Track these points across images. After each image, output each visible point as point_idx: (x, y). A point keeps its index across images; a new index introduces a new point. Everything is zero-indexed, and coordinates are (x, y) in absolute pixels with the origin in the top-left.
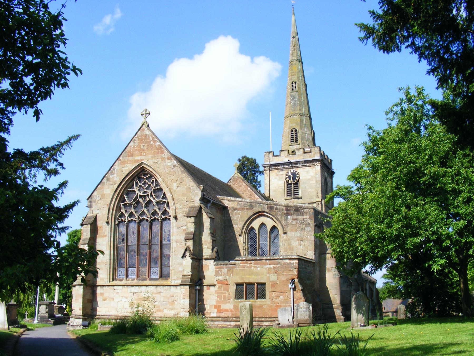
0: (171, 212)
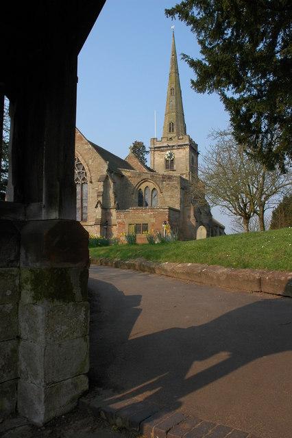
0: (88, 179)
